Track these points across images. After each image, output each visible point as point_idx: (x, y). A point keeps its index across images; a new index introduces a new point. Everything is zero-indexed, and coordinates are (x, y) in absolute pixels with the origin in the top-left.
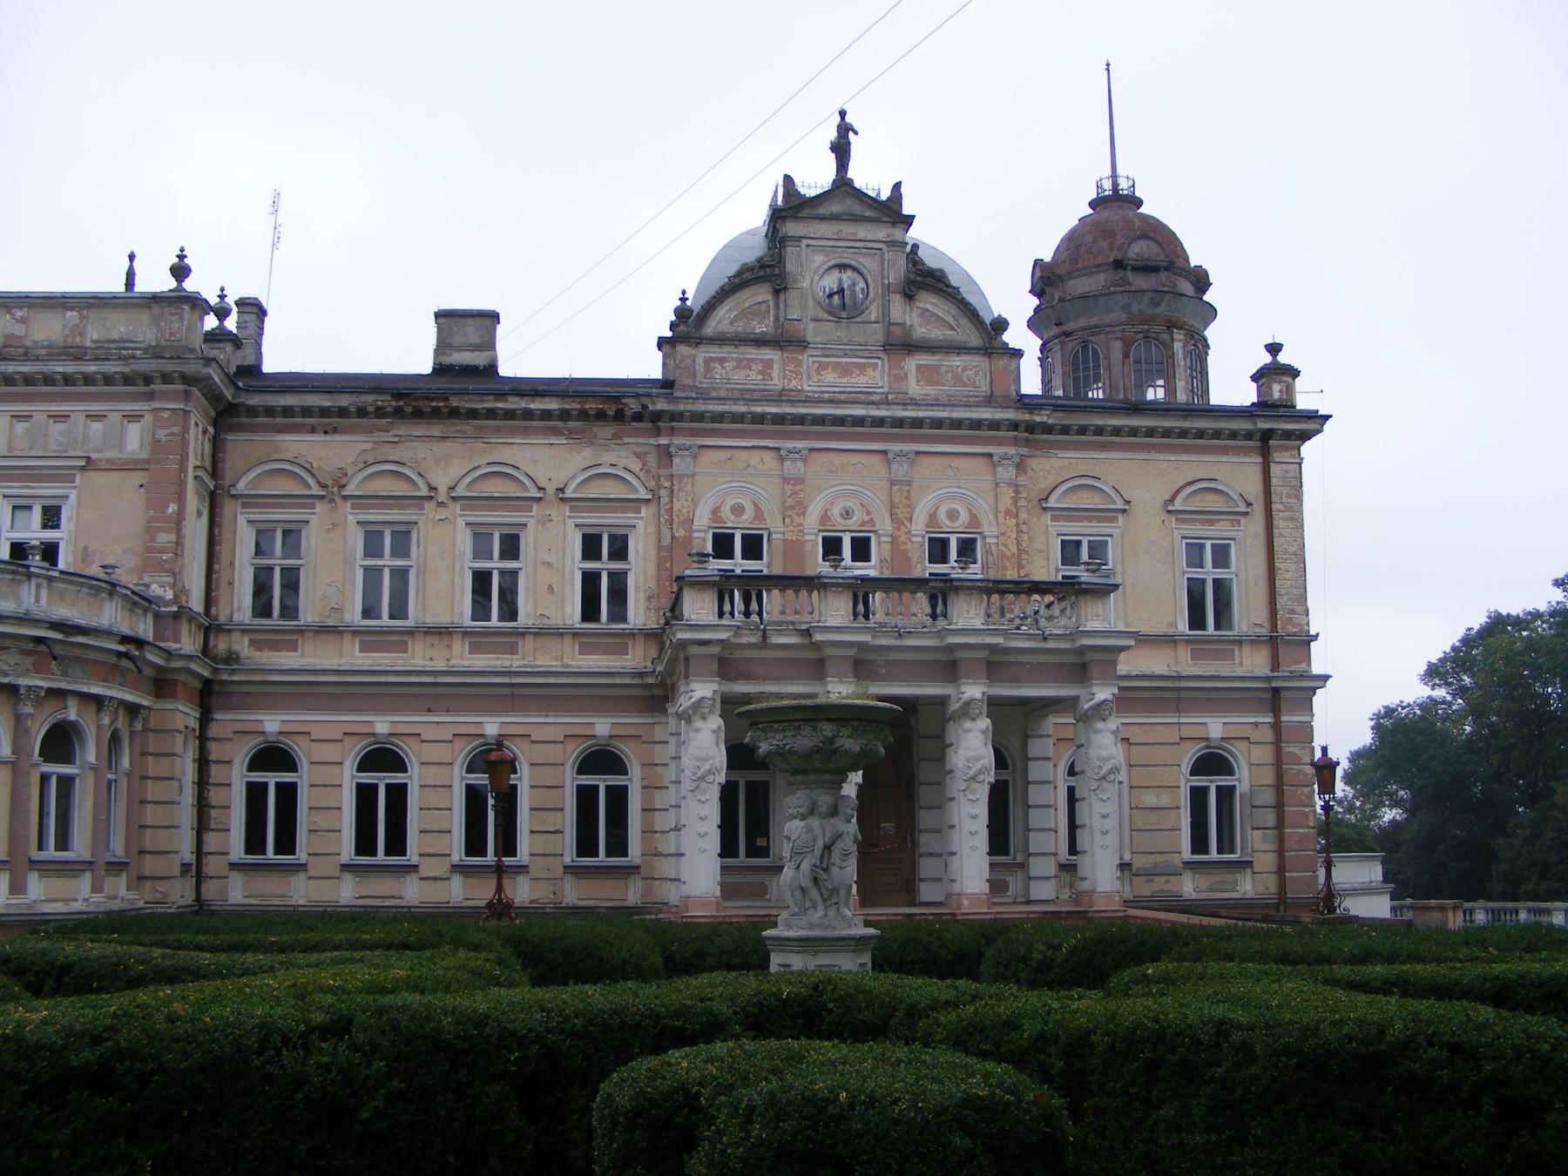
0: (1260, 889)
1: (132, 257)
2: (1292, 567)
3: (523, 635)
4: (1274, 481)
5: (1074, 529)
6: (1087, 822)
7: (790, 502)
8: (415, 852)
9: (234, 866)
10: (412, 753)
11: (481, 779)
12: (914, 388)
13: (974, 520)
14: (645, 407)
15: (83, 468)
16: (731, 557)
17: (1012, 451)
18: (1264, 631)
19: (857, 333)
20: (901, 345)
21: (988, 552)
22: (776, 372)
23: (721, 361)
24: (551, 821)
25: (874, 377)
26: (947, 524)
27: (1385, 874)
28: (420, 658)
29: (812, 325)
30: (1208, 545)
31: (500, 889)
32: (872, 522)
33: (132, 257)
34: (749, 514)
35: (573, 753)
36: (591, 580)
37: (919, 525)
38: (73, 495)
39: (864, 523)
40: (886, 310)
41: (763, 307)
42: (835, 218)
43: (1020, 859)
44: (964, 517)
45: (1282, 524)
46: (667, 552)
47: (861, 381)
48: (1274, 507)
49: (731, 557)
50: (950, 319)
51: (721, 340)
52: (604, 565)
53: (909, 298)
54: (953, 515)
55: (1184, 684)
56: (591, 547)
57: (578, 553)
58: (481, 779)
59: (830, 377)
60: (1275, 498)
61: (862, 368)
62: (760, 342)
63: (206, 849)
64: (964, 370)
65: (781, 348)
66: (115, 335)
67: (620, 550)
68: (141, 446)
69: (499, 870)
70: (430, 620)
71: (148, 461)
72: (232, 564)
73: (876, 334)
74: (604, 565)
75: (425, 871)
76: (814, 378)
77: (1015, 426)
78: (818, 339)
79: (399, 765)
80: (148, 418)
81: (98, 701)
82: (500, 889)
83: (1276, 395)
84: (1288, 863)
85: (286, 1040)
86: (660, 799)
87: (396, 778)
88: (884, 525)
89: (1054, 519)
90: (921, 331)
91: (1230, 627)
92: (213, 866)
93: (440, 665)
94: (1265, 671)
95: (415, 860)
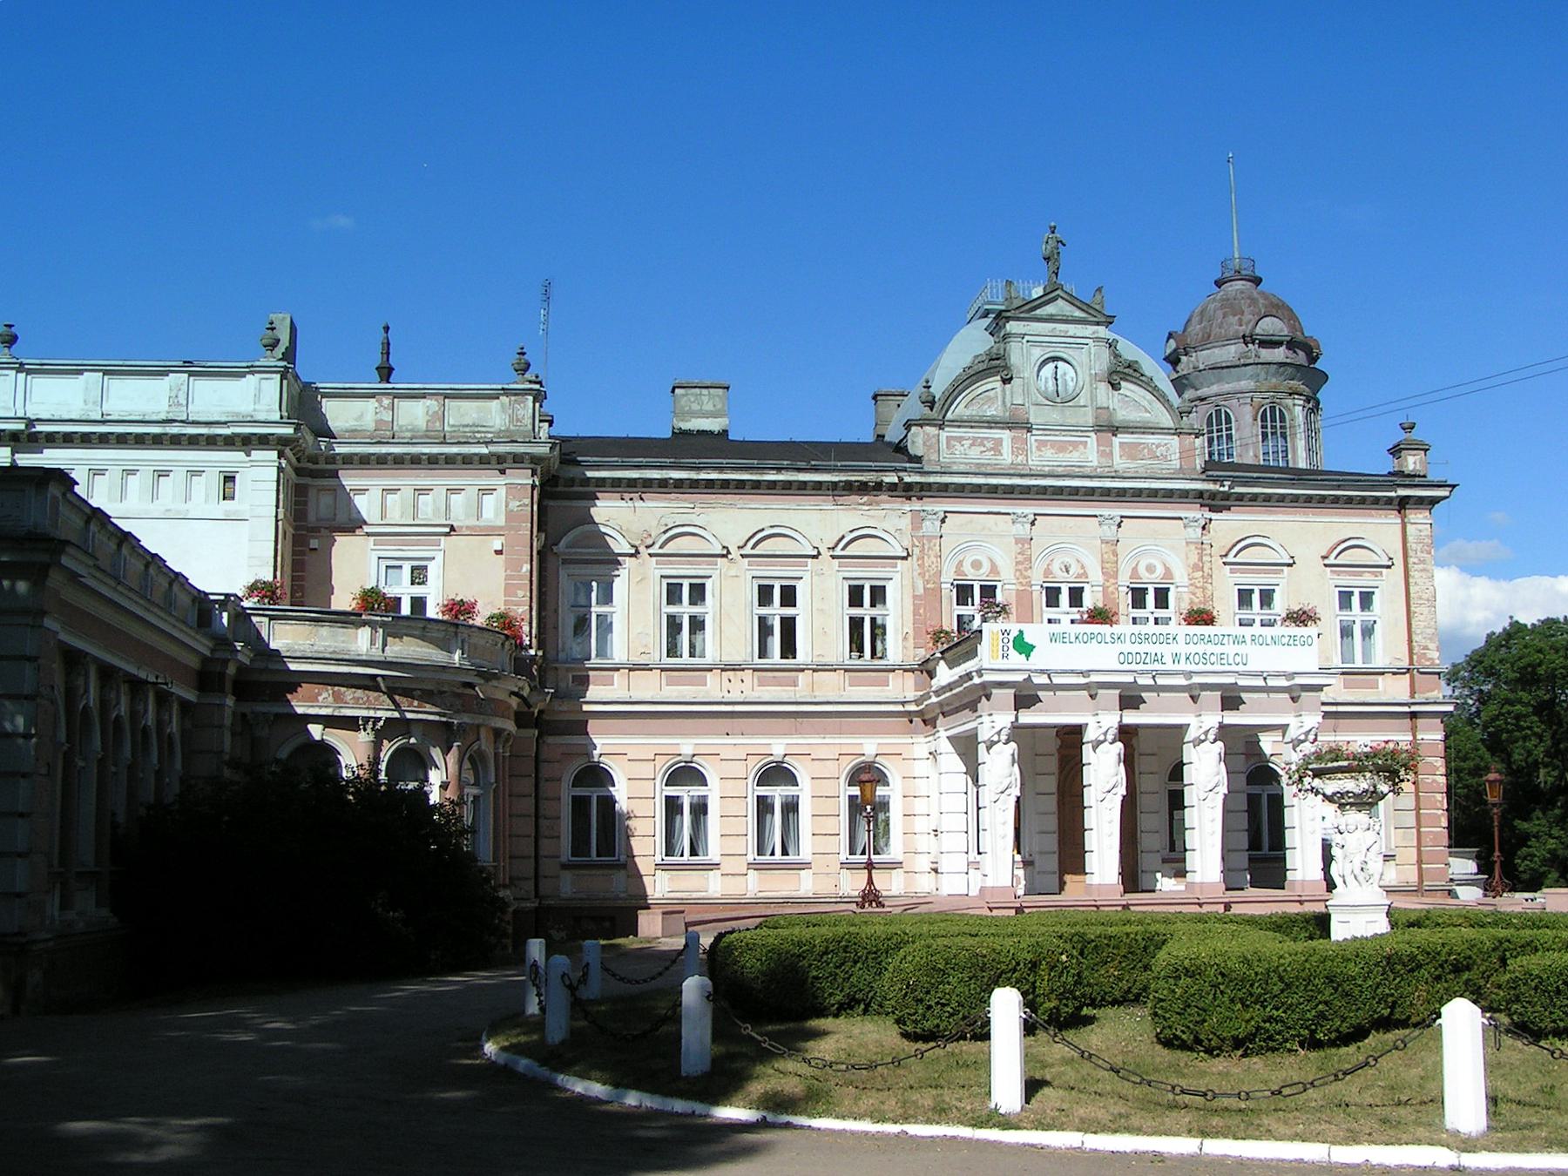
0: (1403, 878)
1: (387, 329)
2: (1425, 610)
4: (1410, 539)
6: (1296, 824)
7: (1020, 558)
9: (565, 867)
10: (710, 770)
11: (856, 791)
12: (1120, 463)
13: (1168, 573)
15: (447, 534)
18: (1405, 664)
21: (1179, 599)
22: (1006, 448)
24: (829, 825)
25: (1089, 454)
27: (1479, 866)
28: (714, 688)
29: (1033, 409)
31: (870, 881)
32: (1085, 574)
33: (387, 329)
35: (662, 767)
37: (1124, 579)
38: (439, 556)
39: (1079, 576)
40: (1093, 398)
42: (1050, 319)
43: (623, 858)
44: (1160, 571)
45: (1417, 574)
46: (927, 599)
47: (1073, 457)
48: (1411, 560)
51: (960, 423)
55: (1341, 709)
56: (855, 597)
58: (856, 791)
59: (1049, 453)
60: (1411, 553)
62: (992, 423)
63: (541, 853)
67: (878, 595)
68: (497, 515)
69: (870, 866)
70: (727, 659)
71: (501, 528)
74: (866, 612)
75: (725, 868)
79: (791, 779)
80: (502, 491)
82: (870, 881)
83: (1411, 467)
87: (698, 791)
88: (1096, 575)
89: (1232, 571)
90: (1123, 414)
92: (548, 867)
95: (716, 860)
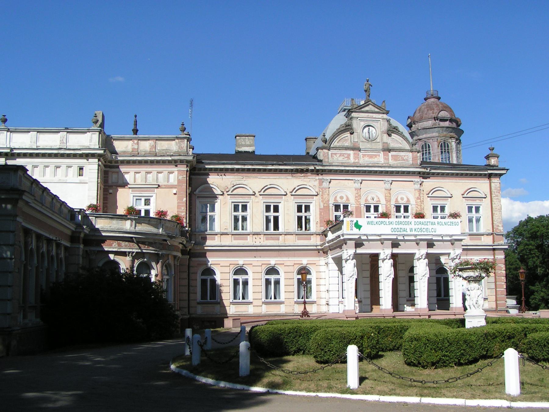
3: (217, 235)
4: (493, 188)
5: (470, 203)
7: (357, 195)
8: (284, 298)
9: (198, 303)
11: (300, 277)
12: (391, 162)
14: (315, 168)
15: (157, 188)
16: (301, 212)
17: (418, 180)
18: (491, 231)
19: (374, 146)
20: (387, 150)
22: (352, 157)
23: (336, 154)
24: (290, 289)
25: (380, 159)
26: (400, 201)
28: (250, 241)
29: (361, 143)
30: (474, 206)
31: (305, 308)
32: (379, 201)
34: (345, 199)
35: (232, 268)
36: (300, 218)
38: (154, 195)
39: (377, 201)
40: (382, 139)
41: (347, 138)
42: (367, 112)
44: (405, 199)
46: (324, 210)
47: (375, 160)
49: (301, 212)
50: (400, 141)
51: (336, 148)
52: (240, 214)
53: (390, 135)
54: (402, 199)
56: (299, 209)
57: (480, 209)
59: (366, 159)
60: (493, 193)
61: (376, 156)
64: (405, 156)
65: (353, 150)
66: (164, 148)
67: (307, 208)
68: (174, 181)
69: (305, 303)
70: (255, 231)
71: (176, 185)
72: (195, 214)
73: (380, 146)
74: (303, 214)
75: (254, 304)
76: (364, 160)
77: (419, 173)
78: (363, 147)
81: (124, 254)
82: (305, 308)
83: (493, 163)
84: (498, 299)
85: (427, 366)
86: (322, 282)
88: (383, 201)
90: (392, 145)
91: (246, 230)
92: (193, 304)
93: (258, 244)
94: (491, 243)
95: (251, 301)
